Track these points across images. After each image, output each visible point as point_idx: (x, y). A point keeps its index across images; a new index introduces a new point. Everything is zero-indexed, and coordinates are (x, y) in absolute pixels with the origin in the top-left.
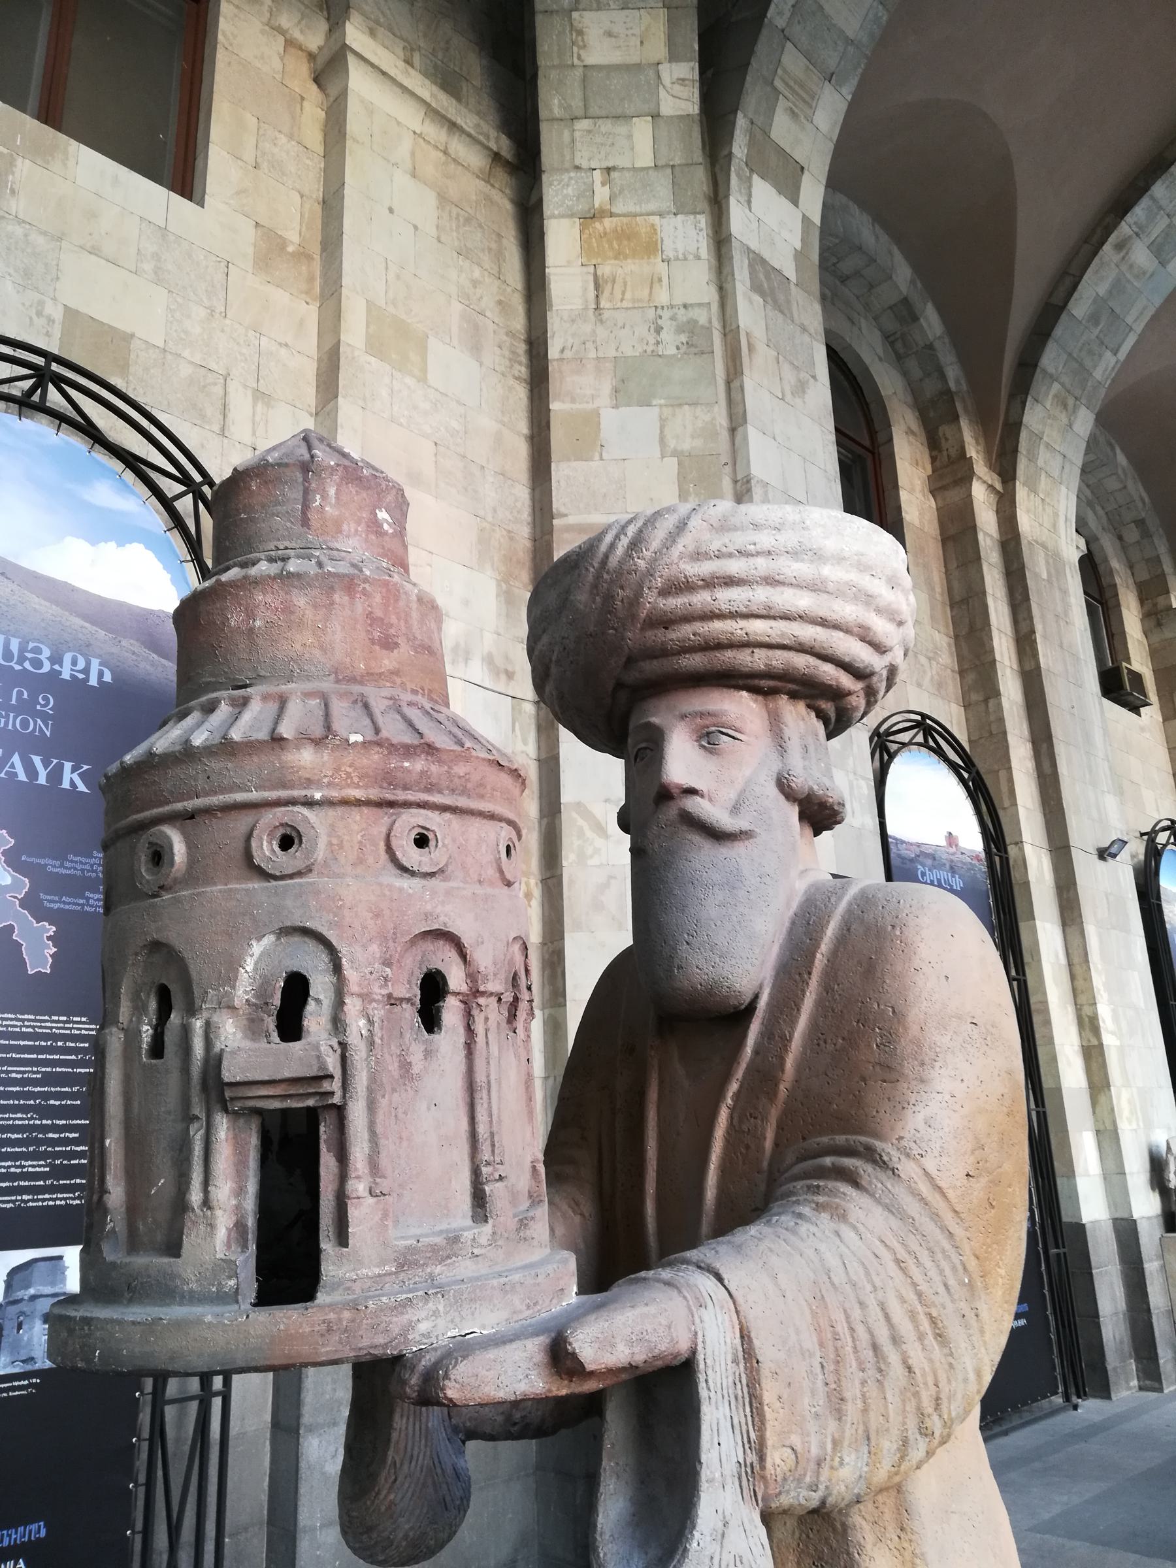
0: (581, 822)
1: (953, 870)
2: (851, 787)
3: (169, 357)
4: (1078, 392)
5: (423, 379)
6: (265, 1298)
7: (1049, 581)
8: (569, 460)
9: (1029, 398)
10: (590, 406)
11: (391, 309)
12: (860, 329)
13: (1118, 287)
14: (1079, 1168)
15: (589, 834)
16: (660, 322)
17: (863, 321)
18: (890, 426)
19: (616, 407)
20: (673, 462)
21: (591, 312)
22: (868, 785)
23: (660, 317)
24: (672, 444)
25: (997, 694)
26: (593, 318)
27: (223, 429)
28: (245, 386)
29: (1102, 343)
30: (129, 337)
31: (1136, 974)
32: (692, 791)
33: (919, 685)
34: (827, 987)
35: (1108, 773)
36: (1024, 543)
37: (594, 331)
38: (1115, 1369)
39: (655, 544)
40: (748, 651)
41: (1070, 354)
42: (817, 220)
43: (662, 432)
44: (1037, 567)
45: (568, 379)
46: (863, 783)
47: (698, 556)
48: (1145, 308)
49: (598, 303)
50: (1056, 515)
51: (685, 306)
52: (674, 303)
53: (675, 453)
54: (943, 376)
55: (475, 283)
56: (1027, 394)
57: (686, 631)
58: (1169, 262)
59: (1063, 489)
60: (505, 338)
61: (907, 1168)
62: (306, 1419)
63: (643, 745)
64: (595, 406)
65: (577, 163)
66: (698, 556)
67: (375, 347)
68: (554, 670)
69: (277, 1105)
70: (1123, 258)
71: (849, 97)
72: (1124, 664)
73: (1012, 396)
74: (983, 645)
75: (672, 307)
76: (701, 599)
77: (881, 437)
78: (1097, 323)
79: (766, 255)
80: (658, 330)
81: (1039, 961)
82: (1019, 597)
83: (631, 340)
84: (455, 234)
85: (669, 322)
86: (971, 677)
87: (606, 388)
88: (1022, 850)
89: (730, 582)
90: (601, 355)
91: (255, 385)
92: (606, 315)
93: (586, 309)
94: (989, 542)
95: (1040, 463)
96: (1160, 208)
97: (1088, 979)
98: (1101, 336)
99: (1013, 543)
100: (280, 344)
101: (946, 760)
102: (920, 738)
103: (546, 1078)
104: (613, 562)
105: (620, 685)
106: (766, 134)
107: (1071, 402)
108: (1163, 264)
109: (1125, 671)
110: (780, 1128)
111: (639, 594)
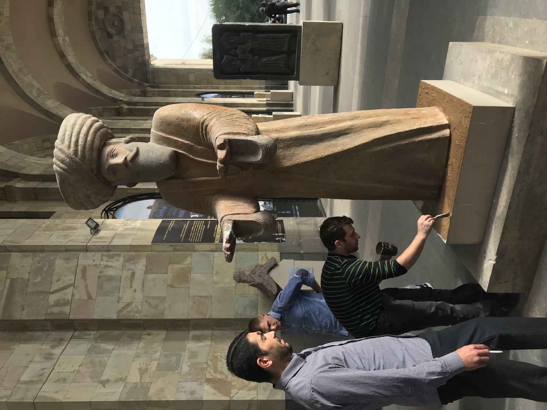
0: (125, 312)
1: (160, 208)
15: (129, 309)
32: (126, 158)
34: (172, 134)
39: (64, 156)
47: (69, 147)
57: (87, 153)
61: (205, 117)
66: (69, 147)
76: (80, 148)
89: (77, 141)
95: (13, 164)
101: (121, 206)
102: (112, 212)
103: (213, 329)
104: (66, 168)
105: (96, 175)
110: (199, 145)
111: (75, 162)
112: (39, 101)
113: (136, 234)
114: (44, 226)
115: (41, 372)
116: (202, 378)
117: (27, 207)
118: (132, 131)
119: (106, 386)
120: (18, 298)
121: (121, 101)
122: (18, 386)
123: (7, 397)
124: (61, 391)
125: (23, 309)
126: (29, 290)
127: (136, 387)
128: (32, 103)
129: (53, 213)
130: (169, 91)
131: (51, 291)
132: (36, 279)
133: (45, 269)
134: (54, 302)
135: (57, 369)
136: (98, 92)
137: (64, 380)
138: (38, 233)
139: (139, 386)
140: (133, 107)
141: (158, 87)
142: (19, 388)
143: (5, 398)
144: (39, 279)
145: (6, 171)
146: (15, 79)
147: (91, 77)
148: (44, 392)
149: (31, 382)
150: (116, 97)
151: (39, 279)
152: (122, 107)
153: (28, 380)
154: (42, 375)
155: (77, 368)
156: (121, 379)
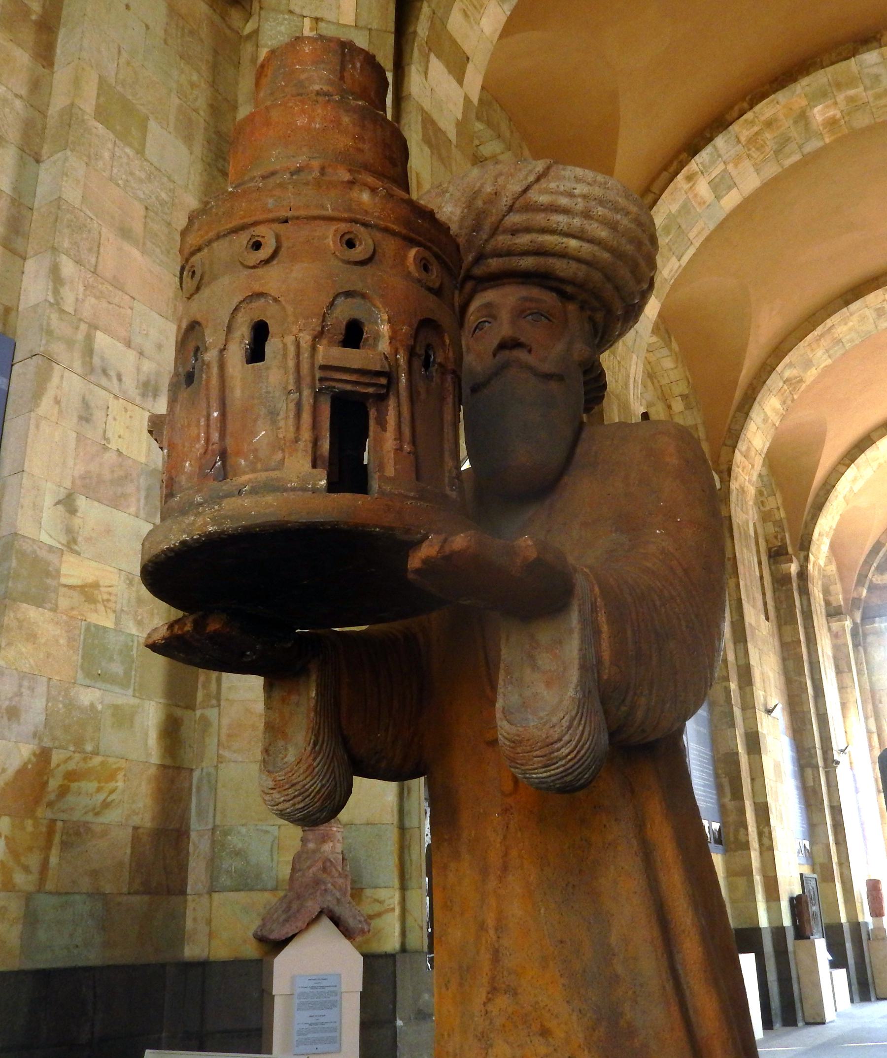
5: (141, 152)
11: (119, 88)
13: (686, 208)
29: (671, 250)
40: (565, 261)
42: (475, 101)
48: (703, 229)
50: (628, 376)
55: (193, 85)
58: (722, 197)
59: (634, 357)
60: (213, 136)
63: (484, 319)
65: (292, 7)
67: (101, 114)
69: (349, 387)
70: (691, 188)
71: (508, 13)
79: (435, 116)
84: (179, 41)
96: (719, 156)
98: (671, 244)
106: (444, 25)
108: (718, 198)
112: (774, 382)
115: (113, 373)
116: (54, 739)
119: (60, 507)
121: (807, 559)
122: (83, 327)
123: (58, 304)
124: (60, 412)
127: (48, 574)
128: (766, 369)
130: (850, 670)
135: (115, 406)
136: (819, 507)
137: (85, 418)
139: (49, 581)
141: (856, 646)
142: (77, 328)
143: (55, 299)
146: (816, 333)
147: (851, 490)
148: (62, 377)
149: (89, 351)
150: (813, 548)
152: (791, 561)
153: (96, 346)
154: (105, 372)
155: (113, 446)
156: (75, 541)
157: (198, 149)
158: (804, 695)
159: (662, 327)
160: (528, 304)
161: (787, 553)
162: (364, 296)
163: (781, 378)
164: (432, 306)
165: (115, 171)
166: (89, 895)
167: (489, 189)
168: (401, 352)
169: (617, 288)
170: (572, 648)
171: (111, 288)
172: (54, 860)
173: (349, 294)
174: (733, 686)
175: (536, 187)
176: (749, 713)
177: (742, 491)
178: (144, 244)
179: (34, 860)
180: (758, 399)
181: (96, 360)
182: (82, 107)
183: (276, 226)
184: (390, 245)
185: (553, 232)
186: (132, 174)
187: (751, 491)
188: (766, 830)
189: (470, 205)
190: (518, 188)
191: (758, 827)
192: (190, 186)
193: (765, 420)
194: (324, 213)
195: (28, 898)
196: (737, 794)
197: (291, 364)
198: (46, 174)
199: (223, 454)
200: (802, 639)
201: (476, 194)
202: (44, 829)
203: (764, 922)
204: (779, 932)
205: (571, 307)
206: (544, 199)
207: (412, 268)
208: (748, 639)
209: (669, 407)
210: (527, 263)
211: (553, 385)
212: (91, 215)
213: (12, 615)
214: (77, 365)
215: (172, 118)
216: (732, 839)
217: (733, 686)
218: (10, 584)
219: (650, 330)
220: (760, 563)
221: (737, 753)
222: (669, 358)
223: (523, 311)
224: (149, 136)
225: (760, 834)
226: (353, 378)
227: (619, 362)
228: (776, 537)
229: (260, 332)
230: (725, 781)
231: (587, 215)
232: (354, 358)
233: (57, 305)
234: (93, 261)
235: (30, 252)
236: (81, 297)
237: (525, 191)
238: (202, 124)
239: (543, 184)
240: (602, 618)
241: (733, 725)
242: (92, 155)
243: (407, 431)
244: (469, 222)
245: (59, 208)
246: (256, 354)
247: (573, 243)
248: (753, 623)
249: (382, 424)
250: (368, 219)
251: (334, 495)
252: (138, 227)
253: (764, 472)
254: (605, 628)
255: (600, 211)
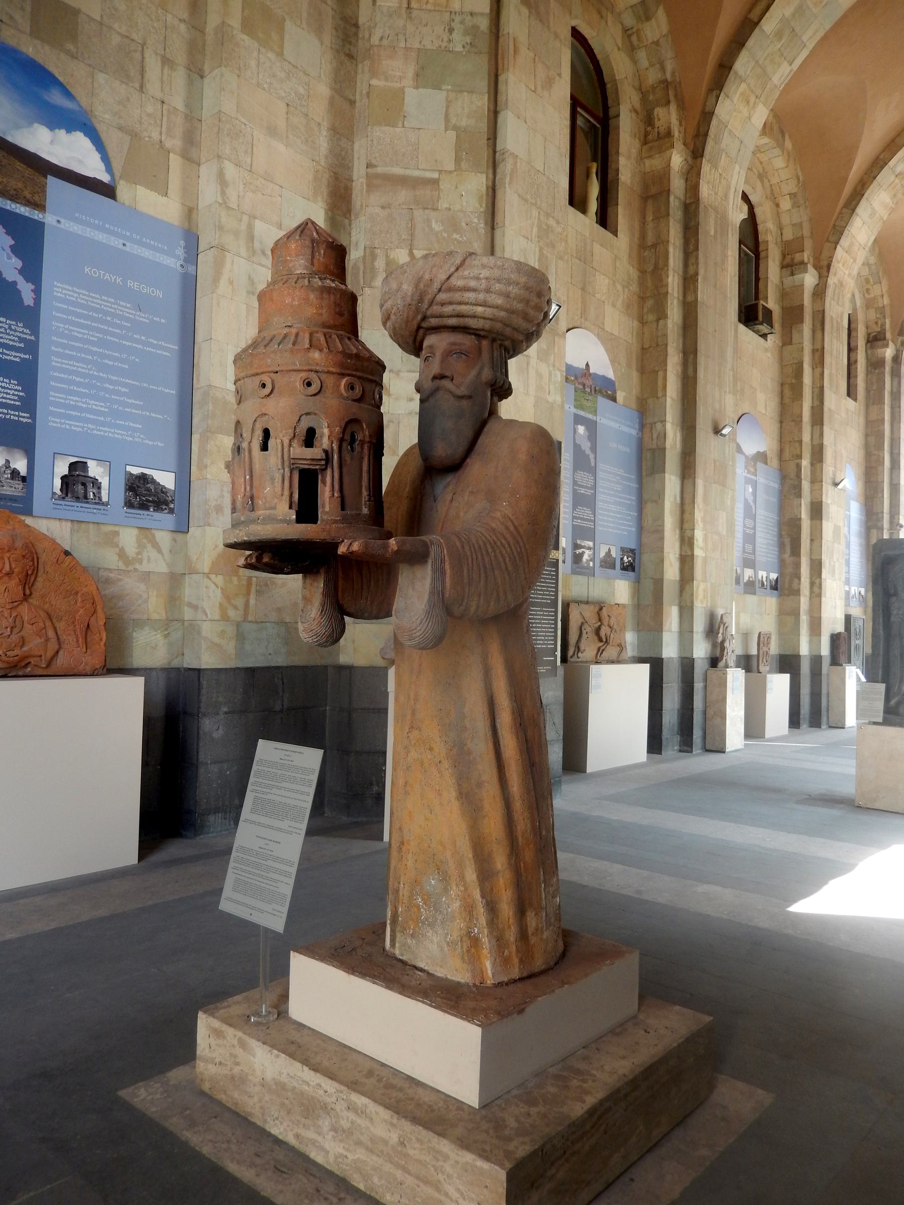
2: (550, 375)
3: (104, 28)
4: (759, 92)
5: (280, 54)
6: (299, 520)
7: (715, 237)
8: (381, 125)
9: (722, 94)
10: (397, 85)
12: (606, 22)
14: (665, 628)
16: (453, 24)
17: (609, 16)
18: (619, 104)
19: (417, 87)
20: (452, 134)
21: (403, 11)
22: (562, 375)
23: (453, 21)
24: (454, 120)
25: (665, 316)
26: (404, 16)
27: (142, 87)
28: (156, 54)
29: (782, 55)
30: (76, 12)
31: (724, 514)
33: (614, 306)
35: (731, 378)
36: (702, 207)
37: (405, 26)
38: (667, 739)
41: (757, 62)
43: (447, 110)
44: (708, 225)
45: (384, 62)
46: (558, 373)
49: (409, 4)
51: (471, 14)
52: (464, 10)
53: (455, 128)
54: (663, 69)
56: (721, 91)
62: (203, 710)
64: (402, 85)
68: (393, 317)
69: (306, 467)
72: (762, 302)
73: (710, 90)
74: (661, 280)
75: (462, 13)
77: (612, 112)
78: (780, 39)
80: (451, 31)
81: (664, 500)
82: (691, 247)
83: (430, 36)
85: (459, 26)
86: (650, 303)
87: (410, 73)
88: (664, 426)
90: (408, 45)
91: (163, 52)
92: (415, 13)
93: (400, 7)
94: (677, 203)
95: (723, 145)
97: (692, 514)
98: (782, 49)
99: (694, 206)
100: (180, 20)
105: (419, 327)
107: (752, 99)
109: (760, 308)
112: (885, 176)
113: (527, 394)
114: (551, 222)
117: (629, 182)
118: (818, 370)
120: (403, 195)
122: (245, 218)
123: (225, 203)
125: (383, 207)
126: (418, 214)
128: (878, 164)
129: (615, 233)
131: (415, 251)
132: (436, 222)
133: (455, 236)
134: (394, 259)
138: (535, 213)
140: (888, 369)
142: (241, 221)
143: (223, 200)
144: (436, 227)
145: (706, 135)
151: (436, 227)
152: (887, 346)
153: (256, 233)
157: (328, 37)
158: (880, 468)
159: (776, 128)
160: (453, 347)
161: (885, 339)
162: (315, 414)
163: (893, 172)
164: (356, 410)
165: (261, 77)
166: (277, 623)
167: (427, 277)
168: (335, 442)
169: (514, 329)
170: (428, 581)
171: (263, 182)
172: (252, 602)
173: (307, 414)
174: (805, 463)
175: (456, 274)
176: (817, 486)
177: (841, 284)
178: (287, 137)
179: (240, 602)
180: (866, 195)
181: (257, 245)
182: (230, 23)
183: (272, 374)
184: (330, 381)
185: (466, 304)
186: (274, 76)
187: (851, 285)
188: (817, 581)
189: (417, 286)
190: (444, 277)
191: (811, 578)
192: (322, 76)
193: (873, 214)
194: (296, 368)
195: (238, 625)
196: (796, 551)
197: (280, 455)
198: (209, 87)
199: (252, 498)
200: (887, 417)
201: (420, 279)
202: (245, 583)
203: (804, 649)
204: (816, 660)
205: (485, 343)
206: (460, 283)
207: (343, 391)
208: (826, 422)
209: (778, 205)
210: (453, 322)
211: (465, 403)
212: (244, 121)
213: (212, 443)
214: (243, 251)
215: (305, 15)
216: (787, 585)
217: (805, 463)
218: (210, 422)
219: (758, 134)
220: (851, 349)
221: (800, 519)
222: (780, 158)
223: (451, 351)
224: (287, 37)
225: (812, 584)
226: (308, 462)
227: (721, 174)
228: (876, 323)
229: (266, 433)
230: (787, 541)
231: (488, 291)
232: (309, 453)
233: (224, 205)
234: (249, 161)
235: (203, 160)
236: (241, 194)
237: (448, 278)
238: (331, 13)
239: (460, 273)
240: (447, 566)
241: (799, 495)
242: (242, 66)
243: (337, 487)
244: (416, 298)
245: (220, 121)
246: (264, 447)
247: (480, 309)
248: (833, 408)
249: (324, 482)
250: (318, 368)
251: (298, 525)
252: (281, 124)
253: (872, 260)
254: (448, 571)
255: (498, 286)
